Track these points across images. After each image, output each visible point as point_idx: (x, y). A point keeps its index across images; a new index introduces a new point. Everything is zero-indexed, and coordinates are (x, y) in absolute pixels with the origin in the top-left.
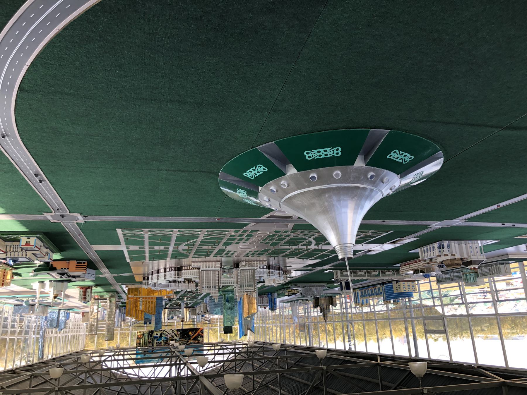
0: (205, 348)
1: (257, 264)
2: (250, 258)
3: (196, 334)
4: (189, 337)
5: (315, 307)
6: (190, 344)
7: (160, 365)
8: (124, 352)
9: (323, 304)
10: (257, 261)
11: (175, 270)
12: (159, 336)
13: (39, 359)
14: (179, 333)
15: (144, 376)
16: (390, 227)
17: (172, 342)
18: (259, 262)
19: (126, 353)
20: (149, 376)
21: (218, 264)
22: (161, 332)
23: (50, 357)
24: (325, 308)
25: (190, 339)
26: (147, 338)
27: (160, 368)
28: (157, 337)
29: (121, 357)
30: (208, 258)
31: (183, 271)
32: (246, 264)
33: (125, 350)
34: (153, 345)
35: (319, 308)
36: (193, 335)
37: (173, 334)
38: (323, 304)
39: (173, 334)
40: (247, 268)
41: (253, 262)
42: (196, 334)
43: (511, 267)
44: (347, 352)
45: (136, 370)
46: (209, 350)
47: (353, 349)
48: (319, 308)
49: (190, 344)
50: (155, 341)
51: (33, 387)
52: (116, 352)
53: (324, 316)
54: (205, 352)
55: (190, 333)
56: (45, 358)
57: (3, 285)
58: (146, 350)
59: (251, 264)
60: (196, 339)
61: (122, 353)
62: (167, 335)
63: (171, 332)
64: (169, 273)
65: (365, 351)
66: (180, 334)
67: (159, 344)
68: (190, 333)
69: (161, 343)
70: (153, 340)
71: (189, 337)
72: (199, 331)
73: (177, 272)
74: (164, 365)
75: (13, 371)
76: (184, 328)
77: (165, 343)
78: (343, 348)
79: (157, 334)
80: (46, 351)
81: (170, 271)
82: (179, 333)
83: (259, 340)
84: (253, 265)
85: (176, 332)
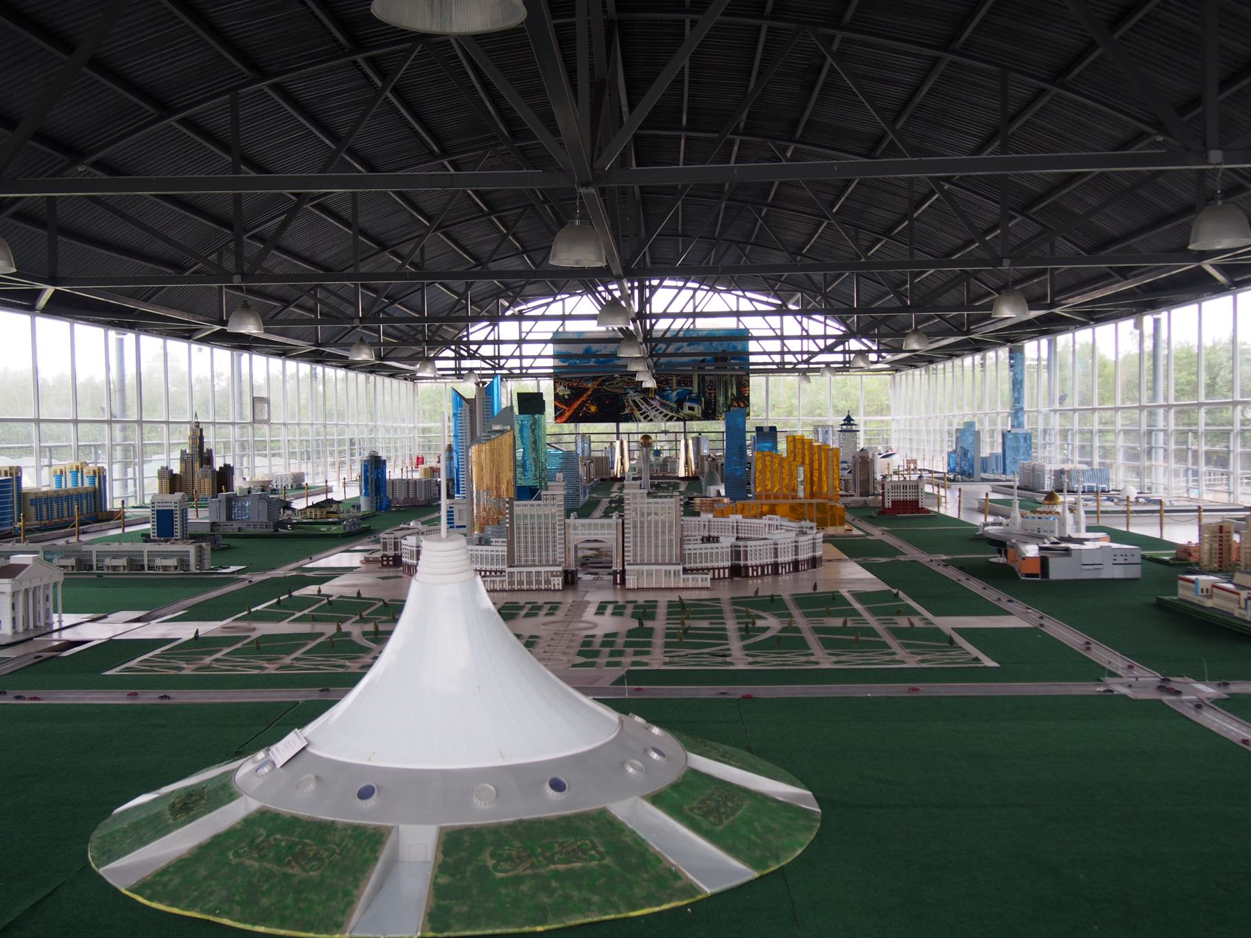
0: (550, 362)
1: (511, 583)
2: (540, 599)
3: (575, 406)
4: (597, 397)
5: (227, 472)
6: (594, 379)
7: (675, 316)
8: (783, 363)
9: (205, 476)
10: (513, 590)
11: (746, 567)
12: (687, 404)
13: (1021, 349)
14: (627, 411)
15: (723, 295)
16: (133, 683)
17: (650, 383)
18: (506, 586)
19: (777, 358)
20: (711, 293)
21: (631, 582)
22: (681, 415)
23: (991, 355)
24: (197, 465)
25: (595, 391)
26: (721, 400)
27: (675, 309)
28: (691, 400)
29: (794, 345)
30: (674, 597)
31: (728, 564)
32: (548, 582)
33: (781, 369)
34: (702, 379)
35: (218, 463)
36: (584, 402)
37: (644, 407)
38: (205, 476)
39: (644, 407)
40: (543, 569)
41: (525, 587)
42: (575, 406)
43: (751, 350)
44: (131, 327)
45: (745, 306)
46: (540, 356)
47: (112, 334)
48: (218, 463)
49: (594, 379)
50: (695, 390)
51: (1044, 272)
52: (803, 362)
53: (201, 438)
54: (550, 349)
55: (593, 409)
56: (1004, 353)
57: (1221, 528)
58: (721, 364)
59: (520, 583)
60: (577, 393)
61: (788, 358)
62: (662, 405)
63: (652, 414)
64: (764, 561)
65: (76, 326)
66: (623, 408)
67: (685, 381)
68: (593, 409)
69: (679, 383)
70: (701, 391)
71: (597, 397)
72: (567, 414)
73: (742, 563)
74: (665, 315)
75: (1093, 320)
76: (611, 426)
77: (667, 382)
78: (146, 340)
79: (691, 409)
80: (1006, 373)
81: (762, 567)
82: (627, 411)
83: (387, 380)
84: (516, 579)
85: (637, 414)
